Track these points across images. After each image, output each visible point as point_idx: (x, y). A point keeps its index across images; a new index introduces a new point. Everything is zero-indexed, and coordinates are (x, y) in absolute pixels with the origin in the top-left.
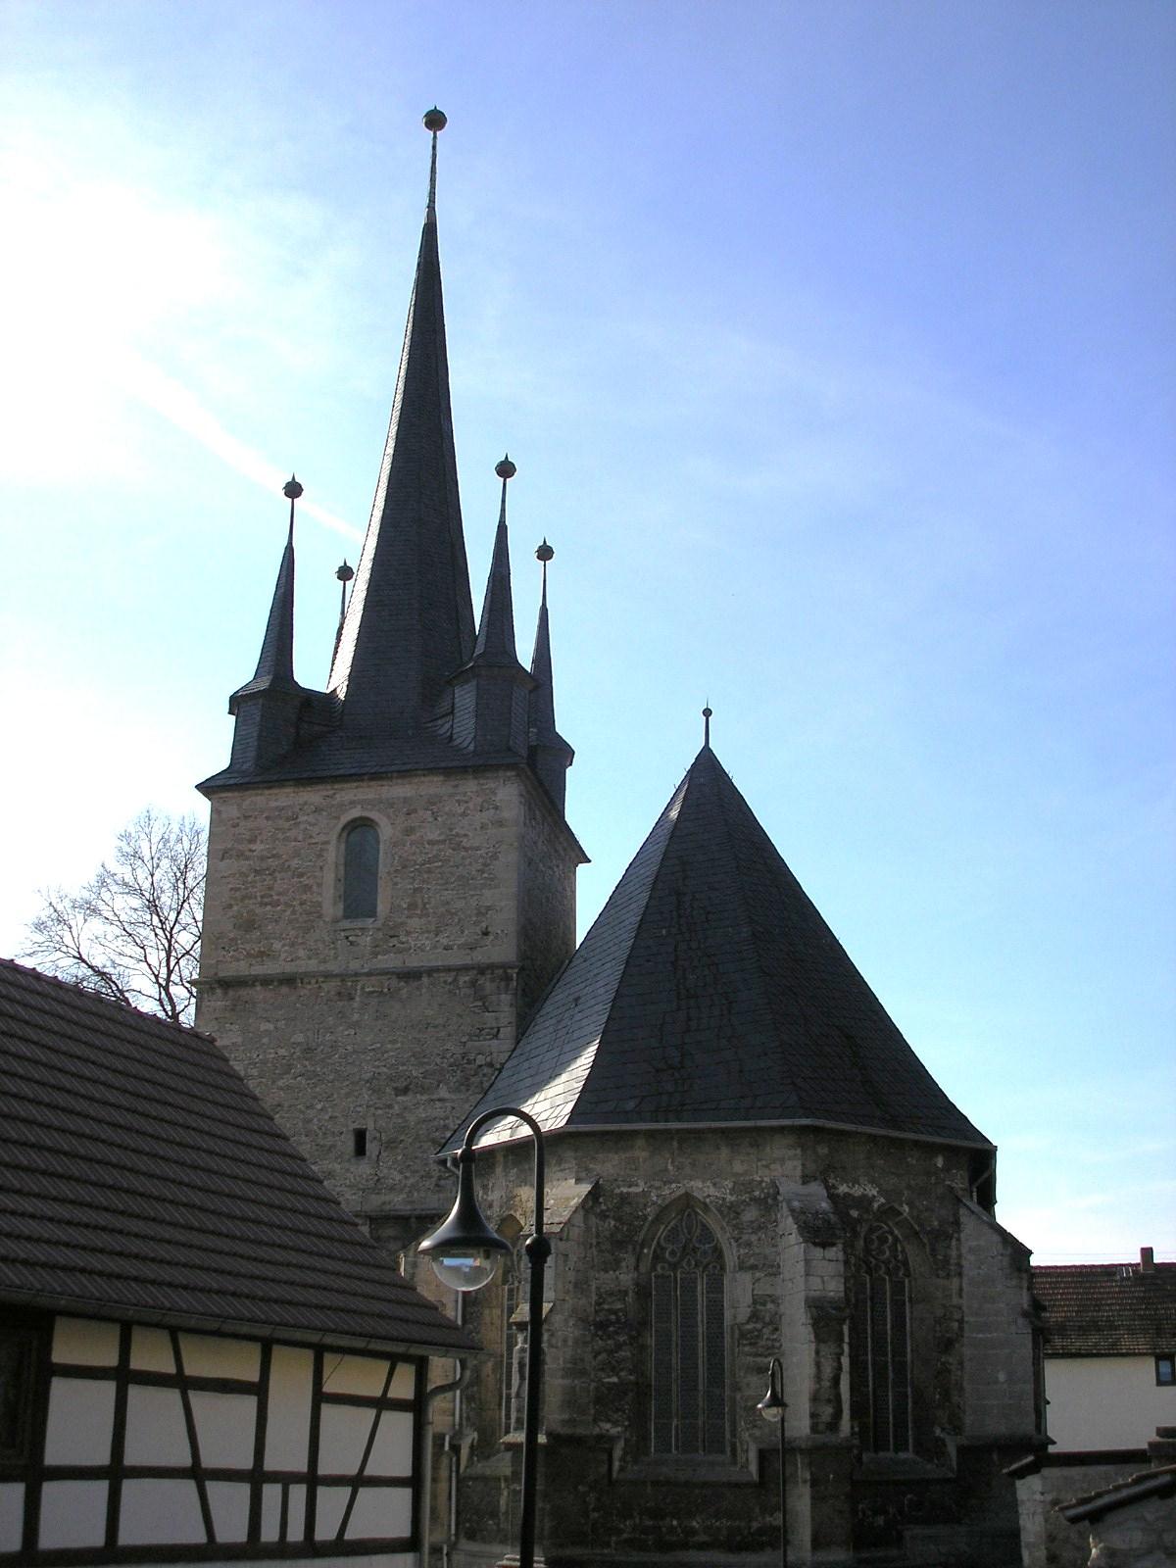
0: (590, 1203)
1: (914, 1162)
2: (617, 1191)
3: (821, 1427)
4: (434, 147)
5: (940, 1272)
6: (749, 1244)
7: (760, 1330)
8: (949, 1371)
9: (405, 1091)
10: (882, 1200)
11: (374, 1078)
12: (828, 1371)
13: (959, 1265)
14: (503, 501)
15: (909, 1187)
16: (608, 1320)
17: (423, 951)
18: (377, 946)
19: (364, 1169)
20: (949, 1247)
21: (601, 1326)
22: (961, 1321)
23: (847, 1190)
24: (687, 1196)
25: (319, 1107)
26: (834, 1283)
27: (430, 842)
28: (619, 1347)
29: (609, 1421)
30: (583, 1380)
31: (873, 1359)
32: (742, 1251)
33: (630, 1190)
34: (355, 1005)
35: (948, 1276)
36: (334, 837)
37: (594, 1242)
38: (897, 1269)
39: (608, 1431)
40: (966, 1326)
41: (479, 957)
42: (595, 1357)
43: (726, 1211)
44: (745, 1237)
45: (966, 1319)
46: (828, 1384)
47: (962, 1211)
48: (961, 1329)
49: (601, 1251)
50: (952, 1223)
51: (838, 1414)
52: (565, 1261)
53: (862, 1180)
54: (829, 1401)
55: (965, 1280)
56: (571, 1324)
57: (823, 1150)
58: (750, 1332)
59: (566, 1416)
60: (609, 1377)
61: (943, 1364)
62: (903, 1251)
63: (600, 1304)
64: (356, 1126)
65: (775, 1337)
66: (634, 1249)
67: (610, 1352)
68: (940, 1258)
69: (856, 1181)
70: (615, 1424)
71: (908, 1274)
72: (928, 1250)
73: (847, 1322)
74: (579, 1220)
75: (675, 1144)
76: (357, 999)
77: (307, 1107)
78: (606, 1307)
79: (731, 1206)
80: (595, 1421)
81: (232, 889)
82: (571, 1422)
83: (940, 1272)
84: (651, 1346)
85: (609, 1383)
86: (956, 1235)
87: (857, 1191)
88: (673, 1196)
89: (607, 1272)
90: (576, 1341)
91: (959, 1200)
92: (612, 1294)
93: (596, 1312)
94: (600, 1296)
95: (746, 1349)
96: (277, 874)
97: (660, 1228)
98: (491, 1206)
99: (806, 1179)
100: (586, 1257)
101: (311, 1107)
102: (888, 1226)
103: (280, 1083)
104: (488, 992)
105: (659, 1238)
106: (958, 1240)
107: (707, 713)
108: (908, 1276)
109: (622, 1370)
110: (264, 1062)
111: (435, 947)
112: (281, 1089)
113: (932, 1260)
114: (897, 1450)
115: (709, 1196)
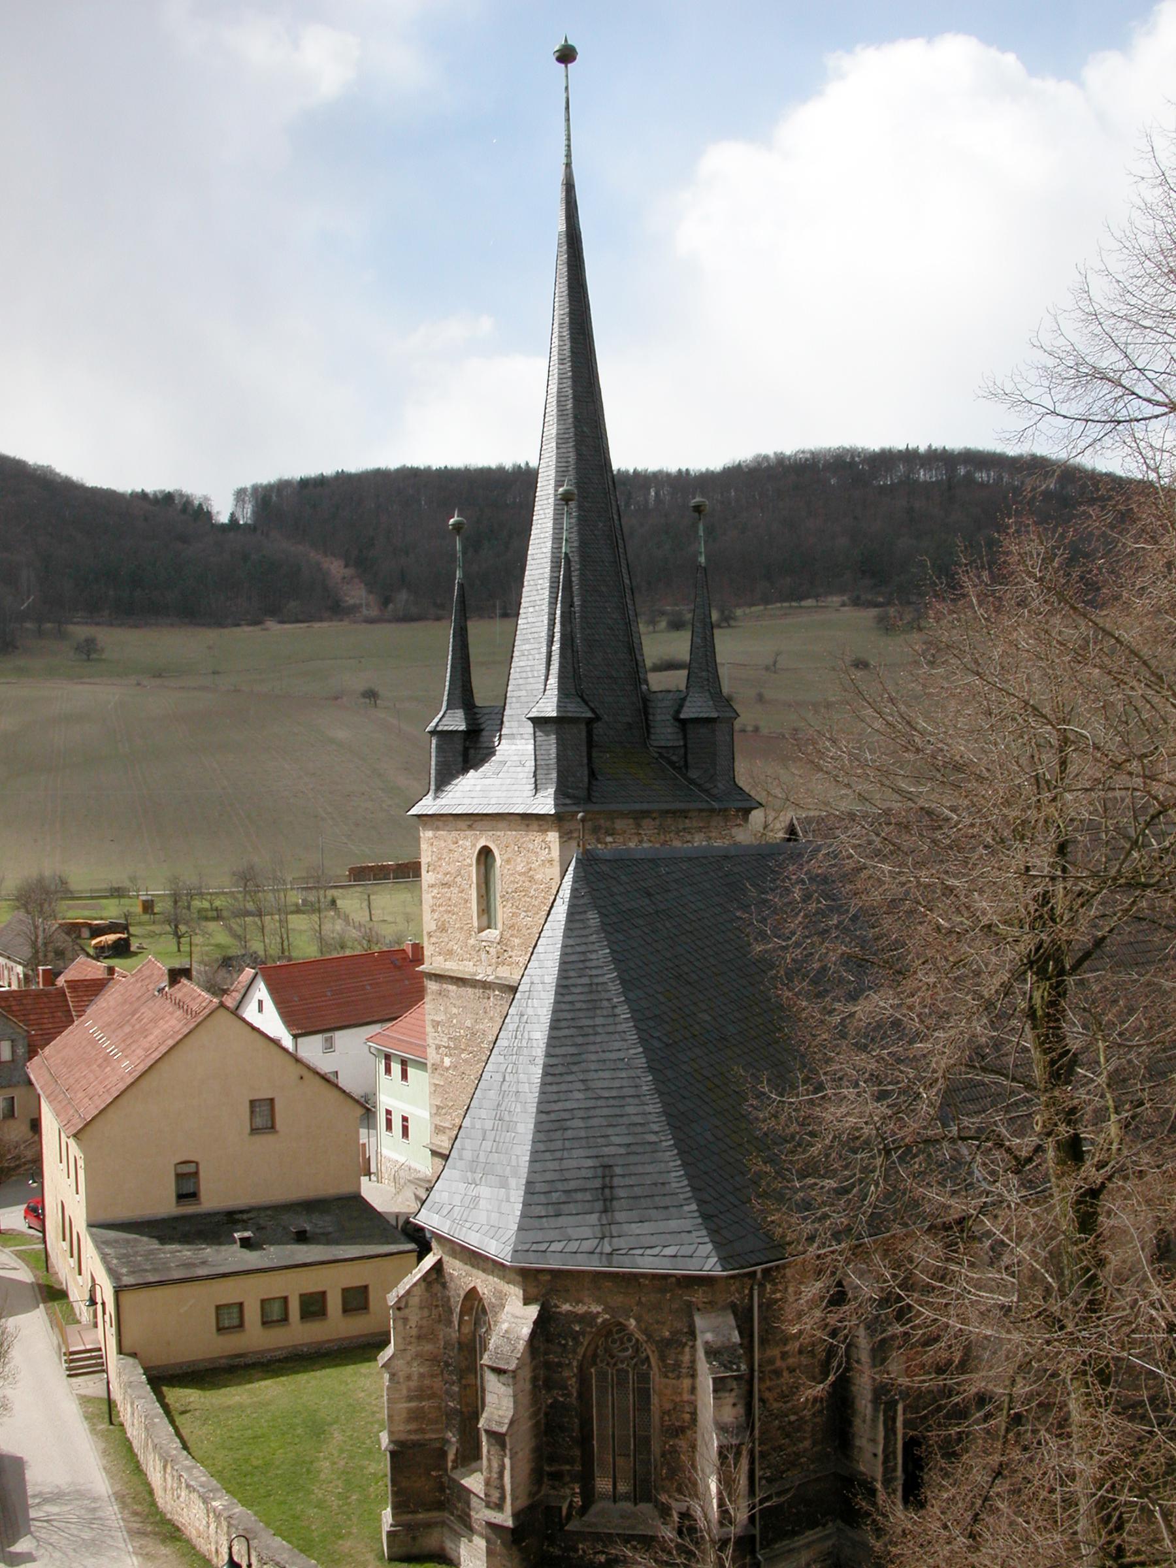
0: (434, 1276)
5: (670, 1375)
10: (607, 1316)
15: (639, 1303)
20: (682, 1353)
23: (570, 1308)
35: (678, 1377)
51: (503, 1498)
52: (405, 1325)
53: (586, 1299)
59: (413, 1426)
74: (418, 1291)
83: (670, 1375)
86: (690, 1343)
87: (581, 1309)
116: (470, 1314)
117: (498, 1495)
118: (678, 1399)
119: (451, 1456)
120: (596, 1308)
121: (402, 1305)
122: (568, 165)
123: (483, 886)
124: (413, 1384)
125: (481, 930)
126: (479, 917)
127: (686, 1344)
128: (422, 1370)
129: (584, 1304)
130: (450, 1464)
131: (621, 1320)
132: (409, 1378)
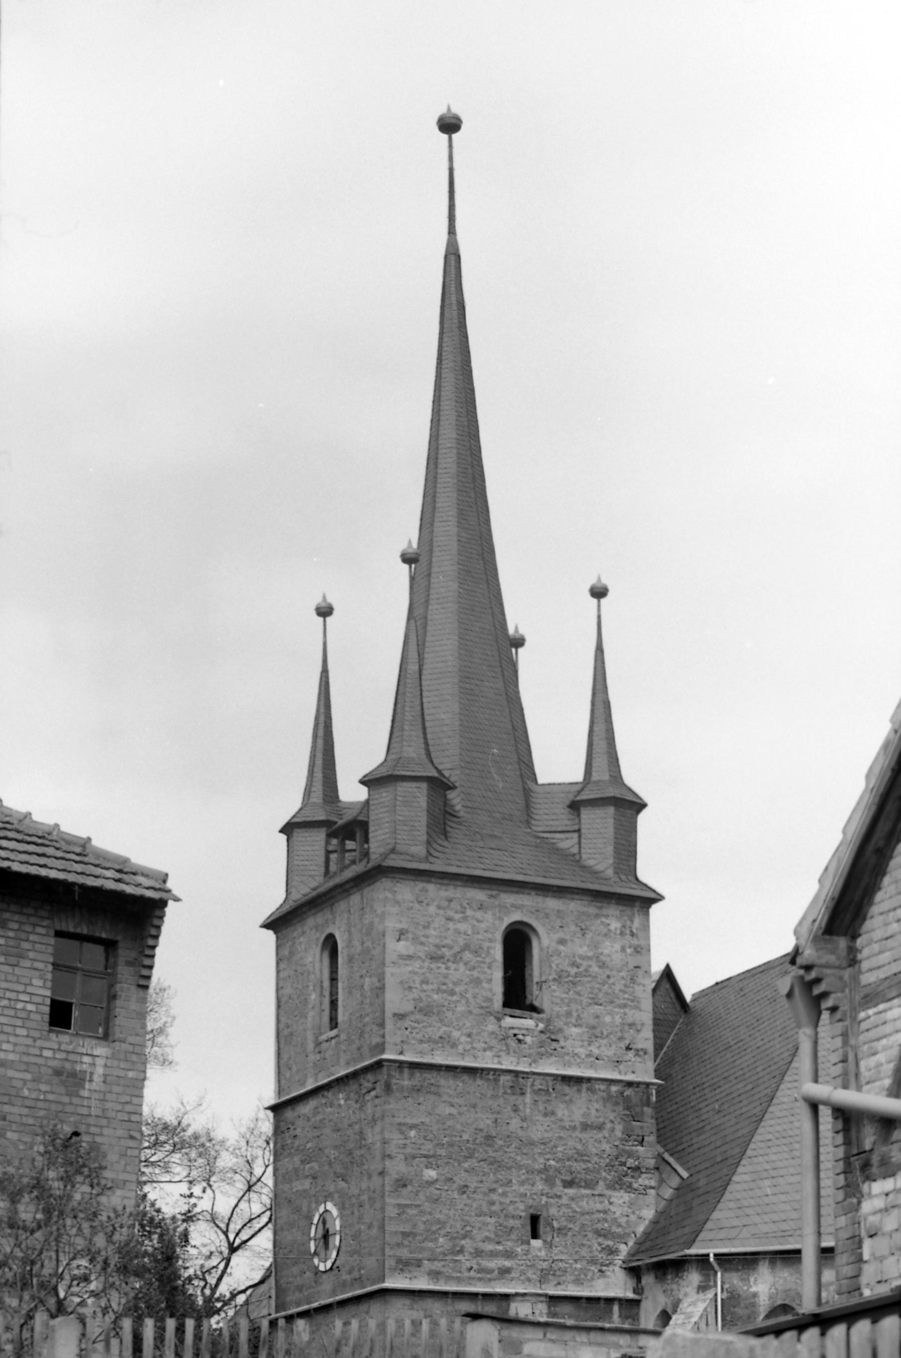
9: (568, 1184)
103: (466, 1165)
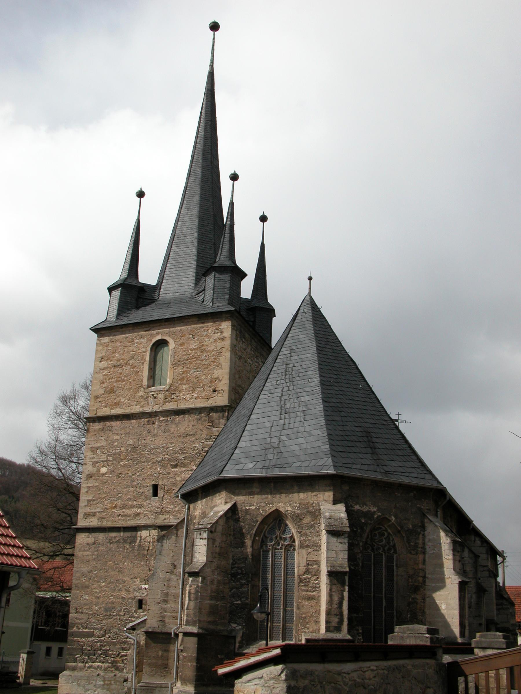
0: (230, 514)
1: (399, 495)
2: (244, 508)
3: (331, 628)
4: (214, 39)
5: (412, 552)
6: (306, 535)
7: (309, 579)
8: (417, 603)
9: (176, 466)
10: (379, 514)
11: (162, 460)
12: (336, 598)
13: (424, 548)
14: (233, 191)
16: (237, 572)
17: (186, 400)
18: (166, 399)
19: (155, 502)
20: (418, 538)
21: (234, 575)
22: (424, 577)
23: (359, 508)
24: (277, 510)
25: (138, 474)
26: (342, 554)
27: (191, 350)
28: (242, 585)
29: (235, 623)
30: (222, 602)
31: (374, 596)
32: (302, 538)
33: (251, 508)
34: (156, 426)
35: (417, 553)
36: (149, 349)
37: (232, 533)
38: (389, 549)
39: (235, 628)
40: (427, 580)
41: (211, 403)
42: (230, 591)
43: (295, 517)
44: (304, 531)
45: (427, 576)
46: (336, 606)
47: (426, 520)
48: (424, 582)
49: (235, 538)
50: (420, 526)
51: (341, 622)
54: (336, 615)
55: (427, 556)
56: (216, 573)
57: (346, 488)
58: (305, 579)
59: (211, 619)
60: (237, 601)
61: (413, 598)
62: (393, 540)
63: (234, 564)
64: (153, 483)
65: (317, 582)
66: (251, 537)
67: (237, 588)
68: (413, 544)
69: (364, 504)
70: (239, 625)
71: (395, 552)
72: (405, 540)
73: (348, 574)
74: (222, 522)
75: (272, 485)
76: (156, 423)
77: (133, 475)
78: (236, 565)
79: (298, 515)
80: (229, 622)
81: (104, 375)
82: (214, 623)
83: (412, 552)
84: (259, 586)
85: (236, 604)
86: (422, 533)
87: (365, 509)
88: (270, 511)
89: (238, 548)
90: (219, 582)
91: (424, 515)
92: (239, 560)
93: (232, 568)
94: (234, 560)
95: (303, 588)
96: (124, 367)
97: (264, 528)
98: (195, 517)
99: (335, 502)
100: (226, 541)
101: (135, 474)
102: (384, 527)
103: (121, 463)
104: (214, 419)
105: (265, 532)
106: (424, 535)
107: (310, 279)
108: (396, 553)
109: (243, 597)
110: (114, 454)
111: (191, 398)
112: (121, 466)
113: (407, 545)
114: (374, 642)
115: (288, 510)
116: (259, 537)
117: (337, 620)
118: (416, 568)
119: (238, 639)
120: (373, 509)
121: (213, 530)
122: (212, 66)
123: (153, 363)
124: (214, 587)
125: (149, 387)
126: (148, 379)
127: (420, 533)
128: (219, 578)
129: (366, 506)
130: (237, 645)
131: (387, 517)
132: (212, 582)
